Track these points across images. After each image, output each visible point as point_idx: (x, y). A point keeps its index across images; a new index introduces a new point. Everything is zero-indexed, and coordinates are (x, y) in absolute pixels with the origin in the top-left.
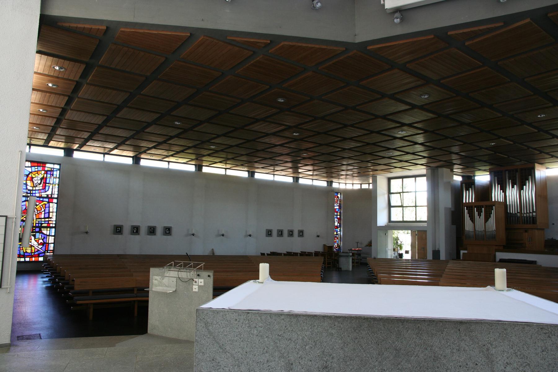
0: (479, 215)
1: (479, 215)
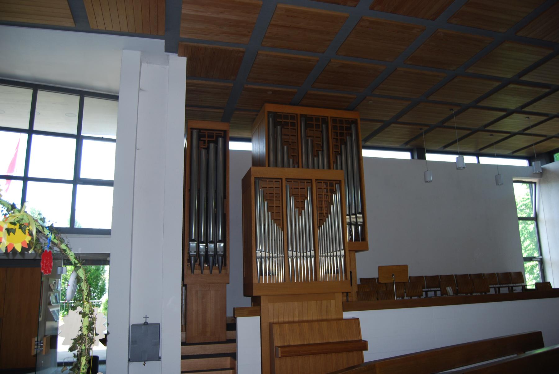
0: (300, 207)
1: (300, 207)
